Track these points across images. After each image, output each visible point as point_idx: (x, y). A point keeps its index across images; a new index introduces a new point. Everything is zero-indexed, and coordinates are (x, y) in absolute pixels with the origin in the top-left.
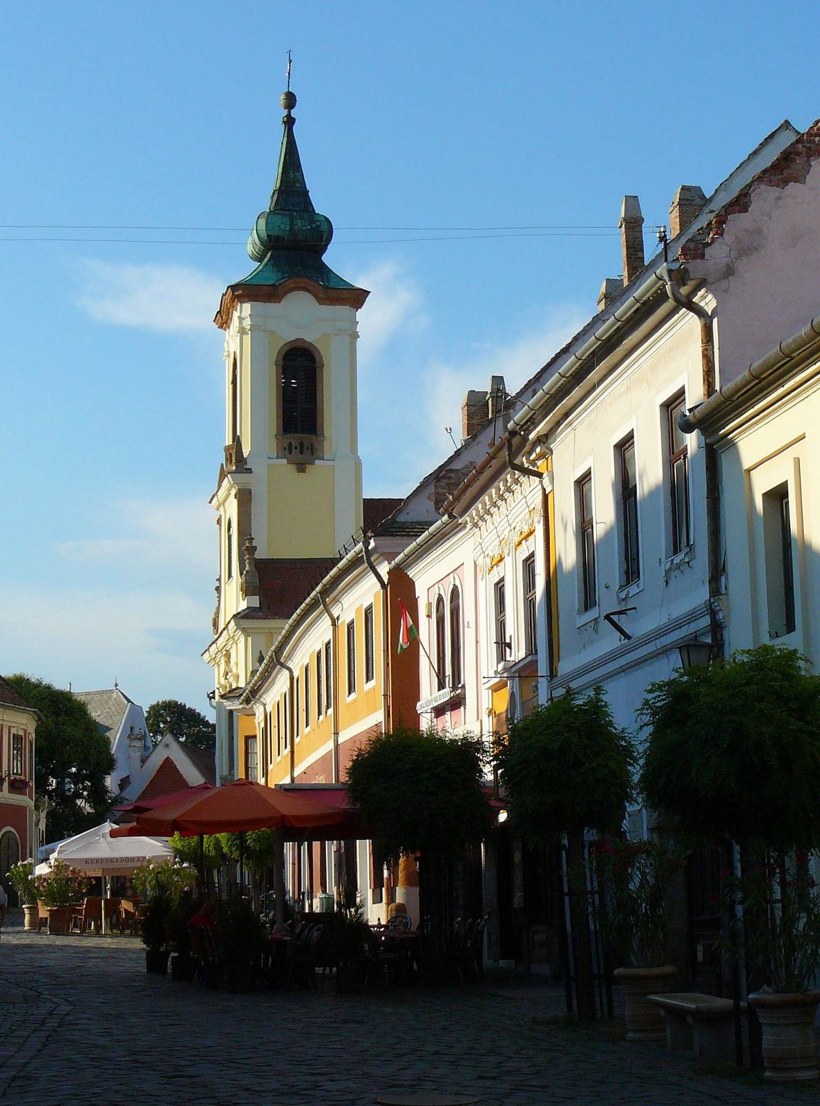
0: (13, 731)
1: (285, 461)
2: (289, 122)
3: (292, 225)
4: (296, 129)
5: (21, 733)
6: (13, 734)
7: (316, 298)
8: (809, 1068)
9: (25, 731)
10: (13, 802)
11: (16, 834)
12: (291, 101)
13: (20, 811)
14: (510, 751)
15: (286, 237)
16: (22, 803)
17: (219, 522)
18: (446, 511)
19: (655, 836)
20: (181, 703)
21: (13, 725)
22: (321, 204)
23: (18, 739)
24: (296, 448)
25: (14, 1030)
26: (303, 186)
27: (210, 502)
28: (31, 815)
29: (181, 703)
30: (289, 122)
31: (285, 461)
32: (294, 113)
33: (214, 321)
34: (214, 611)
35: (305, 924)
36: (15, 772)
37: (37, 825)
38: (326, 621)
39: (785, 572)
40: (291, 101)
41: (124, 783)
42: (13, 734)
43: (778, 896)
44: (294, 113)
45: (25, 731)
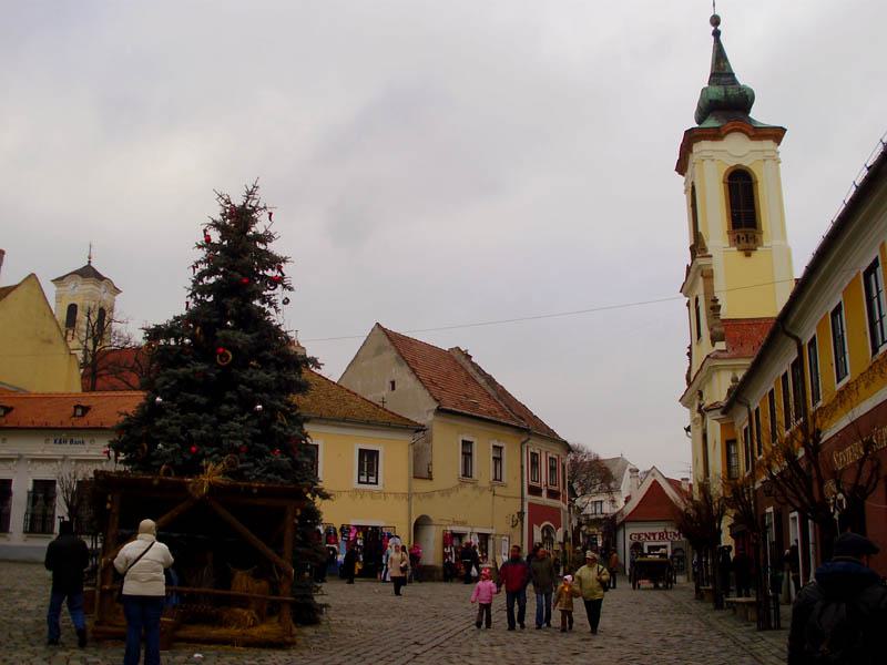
0: (550, 455)
1: (735, 249)
2: (716, 34)
3: (726, 92)
4: (721, 38)
12: (715, 21)
13: (557, 510)
14: (579, 544)
16: (558, 506)
17: (688, 305)
20: (266, 238)
22: (743, 77)
25: (726, 651)
29: (266, 238)
30: (716, 34)
31: (735, 249)
34: (686, 370)
37: (570, 522)
38: (793, 345)
40: (715, 21)
41: (627, 500)
43: (239, 276)
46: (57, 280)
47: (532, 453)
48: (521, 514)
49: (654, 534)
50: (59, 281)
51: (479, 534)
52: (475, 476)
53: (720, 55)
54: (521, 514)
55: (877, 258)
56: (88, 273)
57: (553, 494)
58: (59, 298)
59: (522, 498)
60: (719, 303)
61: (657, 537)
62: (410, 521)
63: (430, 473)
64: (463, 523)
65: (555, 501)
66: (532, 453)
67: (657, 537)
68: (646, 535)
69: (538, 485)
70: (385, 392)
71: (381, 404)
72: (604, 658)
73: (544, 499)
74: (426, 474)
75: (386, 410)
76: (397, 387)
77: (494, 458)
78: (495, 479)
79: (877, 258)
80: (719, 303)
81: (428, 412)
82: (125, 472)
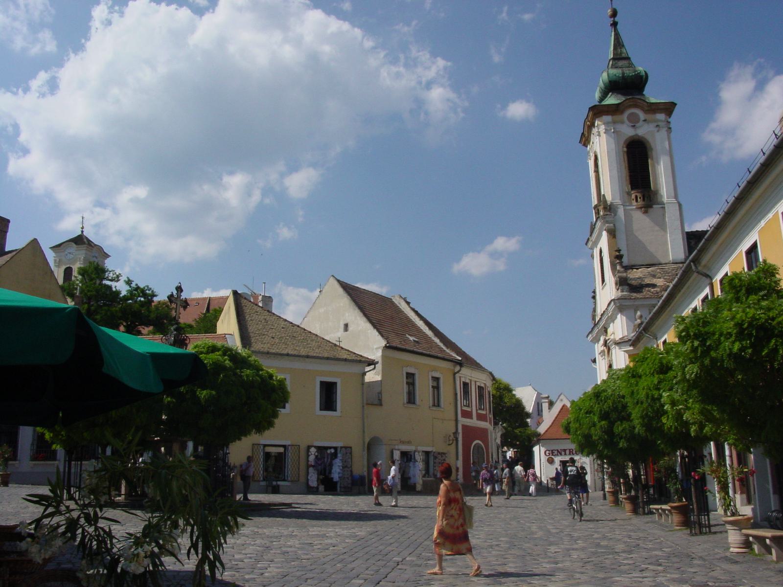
0: (478, 384)
2: (614, 24)
5: (483, 385)
6: (463, 382)
7: (643, 111)
8: (676, 573)
9: (485, 384)
10: (478, 426)
11: (484, 448)
12: (614, 14)
15: (621, 81)
18: (207, 317)
19: (648, 434)
21: (477, 380)
23: (481, 389)
24: (640, 198)
26: (134, 332)
27: (586, 244)
28: (491, 435)
32: (616, 19)
33: (580, 142)
35: (130, 324)
36: (465, 404)
39: (604, 278)
42: (463, 382)
44: (616, 19)
45: (485, 384)
46: (54, 247)
47: (478, 386)
48: (456, 433)
49: (565, 450)
50: (56, 248)
51: (423, 451)
52: (442, 406)
53: (338, 281)
54: (456, 433)
55: (756, 241)
56: (80, 240)
57: (480, 417)
58: (59, 264)
59: (456, 420)
60: (622, 253)
61: (568, 452)
62: (364, 442)
63: (380, 400)
64: (409, 443)
65: (468, 420)
66: (478, 386)
67: (568, 452)
68: (558, 450)
69: (468, 409)
70: (340, 333)
71: (338, 343)
72: (350, 460)
73: (474, 422)
74: (413, 401)
75: (342, 348)
76: (342, 327)
77: (433, 387)
78: (434, 405)
79: (756, 241)
80: (622, 253)
81: (376, 348)
82: (767, 304)
